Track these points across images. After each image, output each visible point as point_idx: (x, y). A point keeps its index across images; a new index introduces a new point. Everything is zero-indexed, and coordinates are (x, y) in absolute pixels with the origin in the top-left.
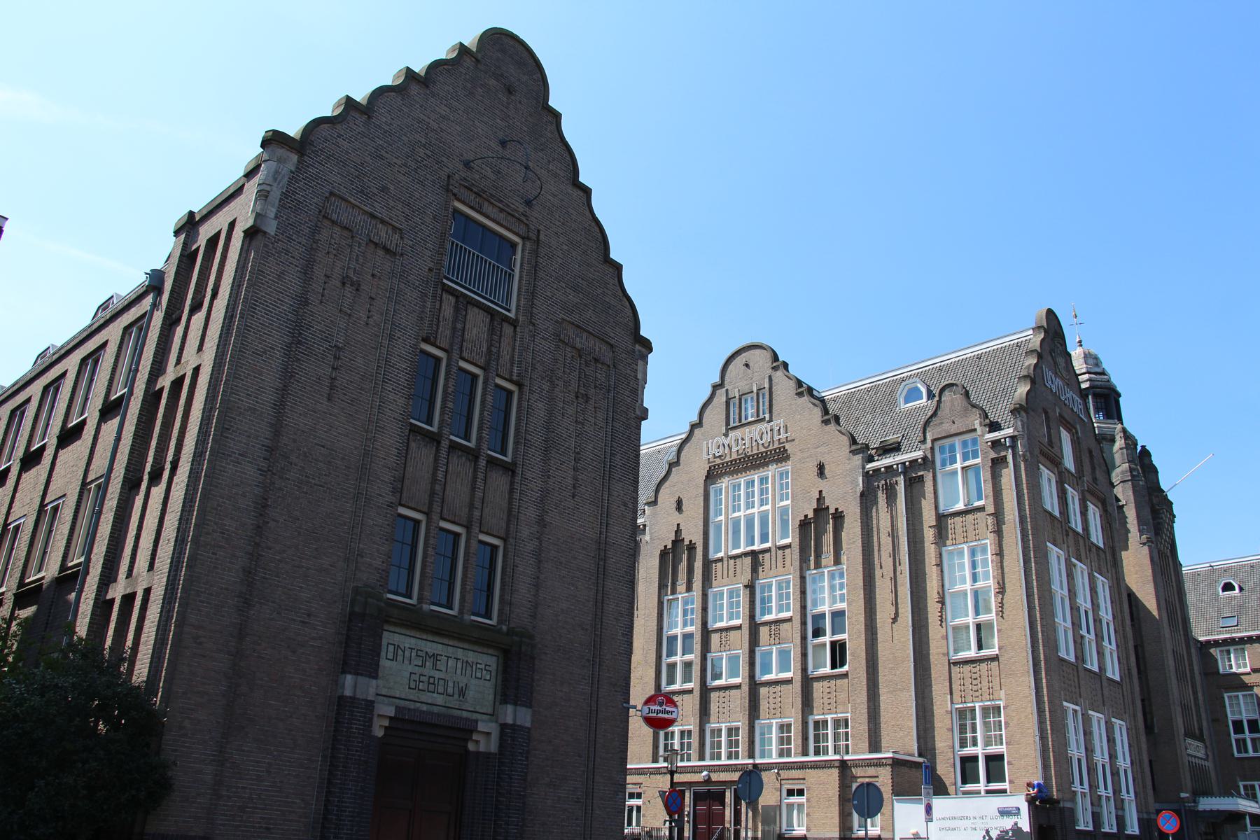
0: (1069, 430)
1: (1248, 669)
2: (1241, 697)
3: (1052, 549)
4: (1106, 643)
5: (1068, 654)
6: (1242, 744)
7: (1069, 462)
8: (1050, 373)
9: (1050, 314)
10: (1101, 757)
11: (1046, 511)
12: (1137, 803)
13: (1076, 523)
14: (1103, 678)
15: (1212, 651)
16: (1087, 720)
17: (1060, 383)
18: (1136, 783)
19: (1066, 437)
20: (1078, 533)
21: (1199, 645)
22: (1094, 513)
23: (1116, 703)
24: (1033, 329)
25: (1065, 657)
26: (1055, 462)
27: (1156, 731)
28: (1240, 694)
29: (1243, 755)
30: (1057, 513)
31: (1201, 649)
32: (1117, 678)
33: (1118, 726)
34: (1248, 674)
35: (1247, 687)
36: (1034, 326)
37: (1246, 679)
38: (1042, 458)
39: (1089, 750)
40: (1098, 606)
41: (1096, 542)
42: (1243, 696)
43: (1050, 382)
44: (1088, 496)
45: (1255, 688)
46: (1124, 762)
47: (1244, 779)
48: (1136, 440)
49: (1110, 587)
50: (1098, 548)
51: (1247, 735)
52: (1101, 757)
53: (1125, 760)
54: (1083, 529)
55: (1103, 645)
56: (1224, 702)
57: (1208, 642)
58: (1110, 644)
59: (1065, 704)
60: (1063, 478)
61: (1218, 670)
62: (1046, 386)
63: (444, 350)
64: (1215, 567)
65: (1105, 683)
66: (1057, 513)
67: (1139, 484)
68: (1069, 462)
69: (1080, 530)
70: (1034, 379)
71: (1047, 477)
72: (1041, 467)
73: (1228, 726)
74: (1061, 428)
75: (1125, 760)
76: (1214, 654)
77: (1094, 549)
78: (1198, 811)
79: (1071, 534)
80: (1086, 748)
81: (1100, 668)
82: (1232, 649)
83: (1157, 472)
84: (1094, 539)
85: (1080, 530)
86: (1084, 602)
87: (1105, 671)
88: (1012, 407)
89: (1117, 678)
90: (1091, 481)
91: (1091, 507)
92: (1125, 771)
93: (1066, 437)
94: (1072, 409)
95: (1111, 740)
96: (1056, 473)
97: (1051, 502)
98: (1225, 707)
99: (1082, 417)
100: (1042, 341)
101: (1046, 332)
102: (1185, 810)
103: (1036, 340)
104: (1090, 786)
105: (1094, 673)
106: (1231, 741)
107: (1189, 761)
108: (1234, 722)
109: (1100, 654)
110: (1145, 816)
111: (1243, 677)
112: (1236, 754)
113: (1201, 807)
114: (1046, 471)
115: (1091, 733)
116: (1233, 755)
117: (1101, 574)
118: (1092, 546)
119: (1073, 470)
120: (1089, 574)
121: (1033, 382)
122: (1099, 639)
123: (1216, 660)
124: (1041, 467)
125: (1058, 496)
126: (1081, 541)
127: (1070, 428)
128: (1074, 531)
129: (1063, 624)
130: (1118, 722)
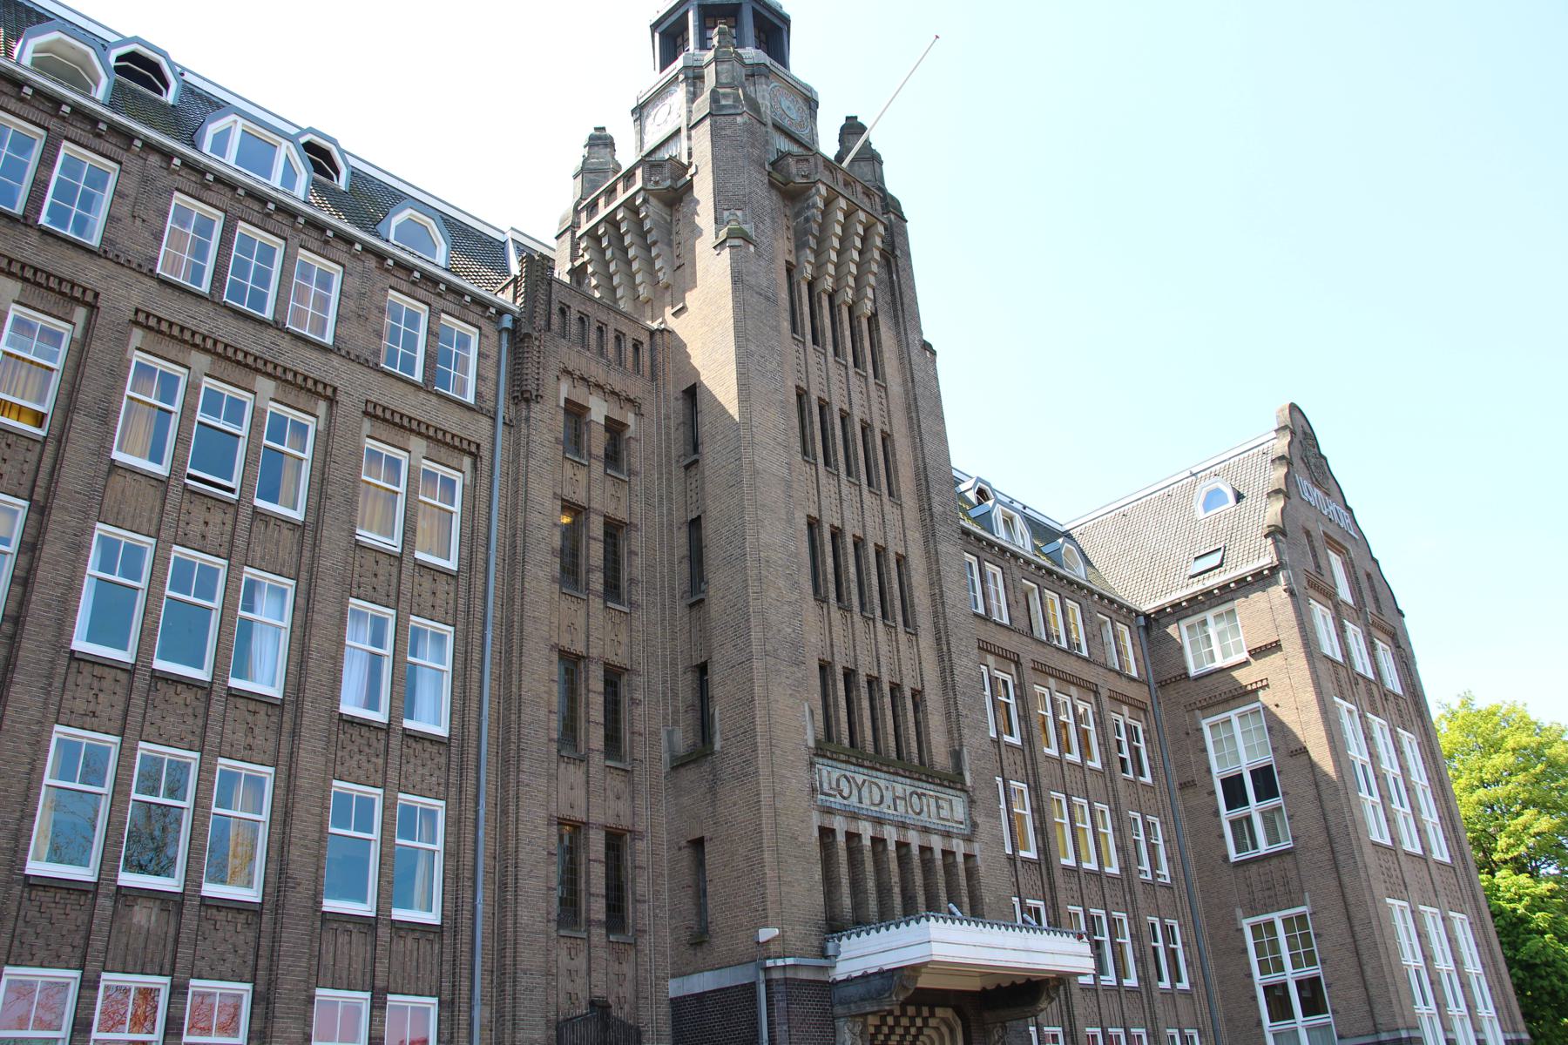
0: (1338, 552)
1: (1244, 656)
2: (1236, 722)
3: (1341, 705)
4: (1396, 805)
5: (1442, 855)
6: (1242, 827)
7: (1344, 593)
8: (1306, 483)
9: (1294, 408)
10: (1444, 964)
11: (1326, 657)
12: (1499, 1020)
13: (1362, 665)
14: (1399, 852)
15: (1171, 629)
16: (1417, 917)
17: (1319, 493)
18: (1494, 992)
19: (1336, 561)
20: (1369, 680)
21: (1142, 621)
22: (1324, 617)
23: (1391, 877)
24: (1276, 431)
25: (1379, 840)
26: (1328, 594)
27: (717, 747)
28: (1233, 714)
29: (1251, 854)
30: (1339, 658)
31: (1147, 628)
32: (1447, 859)
33: (1430, 915)
34: (1246, 663)
35: (1246, 694)
36: (1276, 427)
37: (1244, 677)
38: (1311, 592)
39: (1428, 958)
40: (1408, 770)
41: (1330, 654)
42: (1242, 716)
43: (1307, 494)
44: (1372, 629)
45: (1261, 693)
46: (1474, 967)
47: (1253, 912)
48: (810, 90)
49: (1419, 744)
50: (1396, 696)
51: (1254, 807)
52: (1444, 964)
53: (1446, 962)
54: (1374, 673)
55: (1392, 809)
56: (1203, 739)
57: (1161, 611)
58: (1370, 794)
59: (1389, 901)
60: (1337, 607)
61: (1186, 668)
62: (1303, 499)
63: (420, 501)
64: (1199, 475)
65: (1402, 858)
66: (1339, 658)
67: (735, 123)
68: (1344, 593)
69: (1370, 675)
70: (1286, 492)
71: (1321, 615)
72: (1312, 601)
73: (1213, 793)
74: (1329, 552)
75: (1446, 962)
76: (1176, 636)
77: (1391, 698)
78: (836, 983)
79: (1391, 698)
80: (1424, 956)
81: (1392, 839)
82: (1209, 615)
83: (881, 163)
84: (1359, 669)
85: (1370, 675)
86: (1390, 768)
87: (1431, 852)
88: (1266, 531)
89: (1447, 859)
90: (1375, 612)
91: (1349, 626)
92: (1417, 972)
93: (1336, 561)
94: (1338, 525)
95: (1422, 935)
96: (1332, 607)
97: (1329, 645)
98: (1204, 750)
99: (1352, 533)
100: (1290, 444)
101: (1293, 433)
102: (768, 983)
103: (1281, 445)
104: (1437, 1005)
105: (1387, 848)
106: (1220, 826)
107: (826, 833)
108: (1225, 782)
109: (1391, 820)
110: (1513, 1037)
111: (1235, 674)
112: (1233, 856)
113: (844, 968)
114: (1319, 606)
115: (1427, 936)
116: (1226, 858)
117: (1405, 729)
118: (1387, 695)
119: (1350, 601)
120: (1390, 730)
121: (1287, 496)
122: (1416, 811)
123: (1181, 648)
124: (1312, 601)
125: (1337, 635)
126: (1343, 674)
127: (1340, 549)
128: (1364, 677)
129: (1369, 798)
130: (1397, 902)
